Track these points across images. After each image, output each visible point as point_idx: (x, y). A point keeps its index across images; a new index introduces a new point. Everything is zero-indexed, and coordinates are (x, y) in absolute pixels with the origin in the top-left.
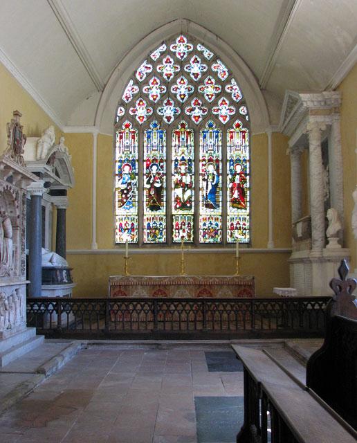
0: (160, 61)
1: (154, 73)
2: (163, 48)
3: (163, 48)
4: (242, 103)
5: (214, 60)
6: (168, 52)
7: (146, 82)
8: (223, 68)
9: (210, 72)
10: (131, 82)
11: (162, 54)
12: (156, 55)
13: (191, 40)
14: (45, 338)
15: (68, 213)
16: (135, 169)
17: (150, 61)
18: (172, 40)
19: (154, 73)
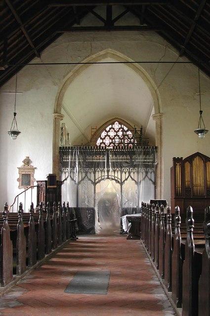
0: (109, 131)
1: (107, 135)
2: (110, 126)
3: (110, 126)
4: (132, 138)
5: (128, 131)
6: (112, 128)
7: (104, 138)
8: (131, 133)
9: (117, 135)
10: (99, 138)
11: (110, 129)
12: (108, 129)
13: (120, 123)
14: (46, 181)
15: (178, 155)
16: (68, 159)
17: (106, 131)
18: (113, 124)
19: (107, 135)
